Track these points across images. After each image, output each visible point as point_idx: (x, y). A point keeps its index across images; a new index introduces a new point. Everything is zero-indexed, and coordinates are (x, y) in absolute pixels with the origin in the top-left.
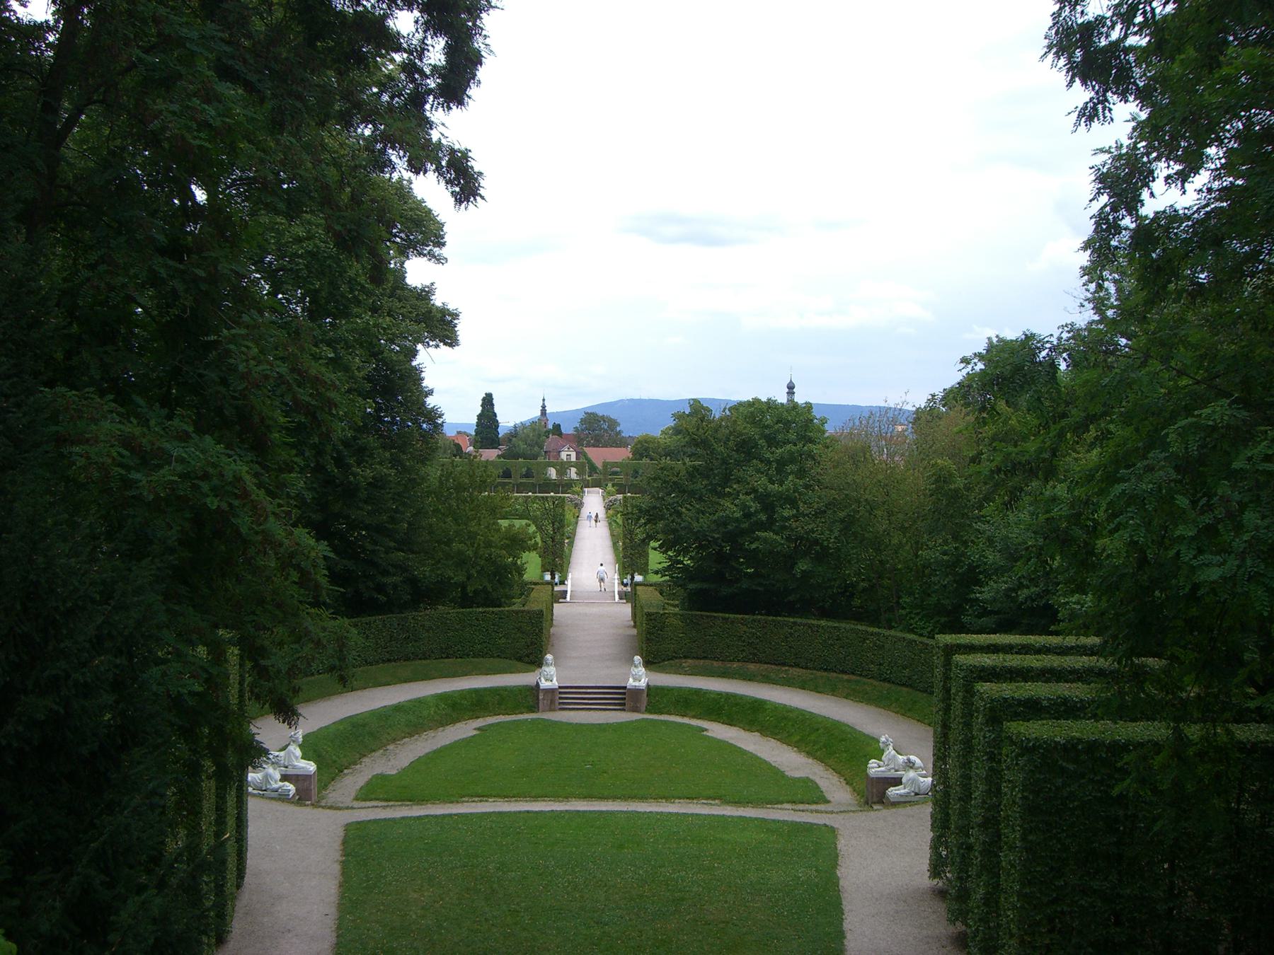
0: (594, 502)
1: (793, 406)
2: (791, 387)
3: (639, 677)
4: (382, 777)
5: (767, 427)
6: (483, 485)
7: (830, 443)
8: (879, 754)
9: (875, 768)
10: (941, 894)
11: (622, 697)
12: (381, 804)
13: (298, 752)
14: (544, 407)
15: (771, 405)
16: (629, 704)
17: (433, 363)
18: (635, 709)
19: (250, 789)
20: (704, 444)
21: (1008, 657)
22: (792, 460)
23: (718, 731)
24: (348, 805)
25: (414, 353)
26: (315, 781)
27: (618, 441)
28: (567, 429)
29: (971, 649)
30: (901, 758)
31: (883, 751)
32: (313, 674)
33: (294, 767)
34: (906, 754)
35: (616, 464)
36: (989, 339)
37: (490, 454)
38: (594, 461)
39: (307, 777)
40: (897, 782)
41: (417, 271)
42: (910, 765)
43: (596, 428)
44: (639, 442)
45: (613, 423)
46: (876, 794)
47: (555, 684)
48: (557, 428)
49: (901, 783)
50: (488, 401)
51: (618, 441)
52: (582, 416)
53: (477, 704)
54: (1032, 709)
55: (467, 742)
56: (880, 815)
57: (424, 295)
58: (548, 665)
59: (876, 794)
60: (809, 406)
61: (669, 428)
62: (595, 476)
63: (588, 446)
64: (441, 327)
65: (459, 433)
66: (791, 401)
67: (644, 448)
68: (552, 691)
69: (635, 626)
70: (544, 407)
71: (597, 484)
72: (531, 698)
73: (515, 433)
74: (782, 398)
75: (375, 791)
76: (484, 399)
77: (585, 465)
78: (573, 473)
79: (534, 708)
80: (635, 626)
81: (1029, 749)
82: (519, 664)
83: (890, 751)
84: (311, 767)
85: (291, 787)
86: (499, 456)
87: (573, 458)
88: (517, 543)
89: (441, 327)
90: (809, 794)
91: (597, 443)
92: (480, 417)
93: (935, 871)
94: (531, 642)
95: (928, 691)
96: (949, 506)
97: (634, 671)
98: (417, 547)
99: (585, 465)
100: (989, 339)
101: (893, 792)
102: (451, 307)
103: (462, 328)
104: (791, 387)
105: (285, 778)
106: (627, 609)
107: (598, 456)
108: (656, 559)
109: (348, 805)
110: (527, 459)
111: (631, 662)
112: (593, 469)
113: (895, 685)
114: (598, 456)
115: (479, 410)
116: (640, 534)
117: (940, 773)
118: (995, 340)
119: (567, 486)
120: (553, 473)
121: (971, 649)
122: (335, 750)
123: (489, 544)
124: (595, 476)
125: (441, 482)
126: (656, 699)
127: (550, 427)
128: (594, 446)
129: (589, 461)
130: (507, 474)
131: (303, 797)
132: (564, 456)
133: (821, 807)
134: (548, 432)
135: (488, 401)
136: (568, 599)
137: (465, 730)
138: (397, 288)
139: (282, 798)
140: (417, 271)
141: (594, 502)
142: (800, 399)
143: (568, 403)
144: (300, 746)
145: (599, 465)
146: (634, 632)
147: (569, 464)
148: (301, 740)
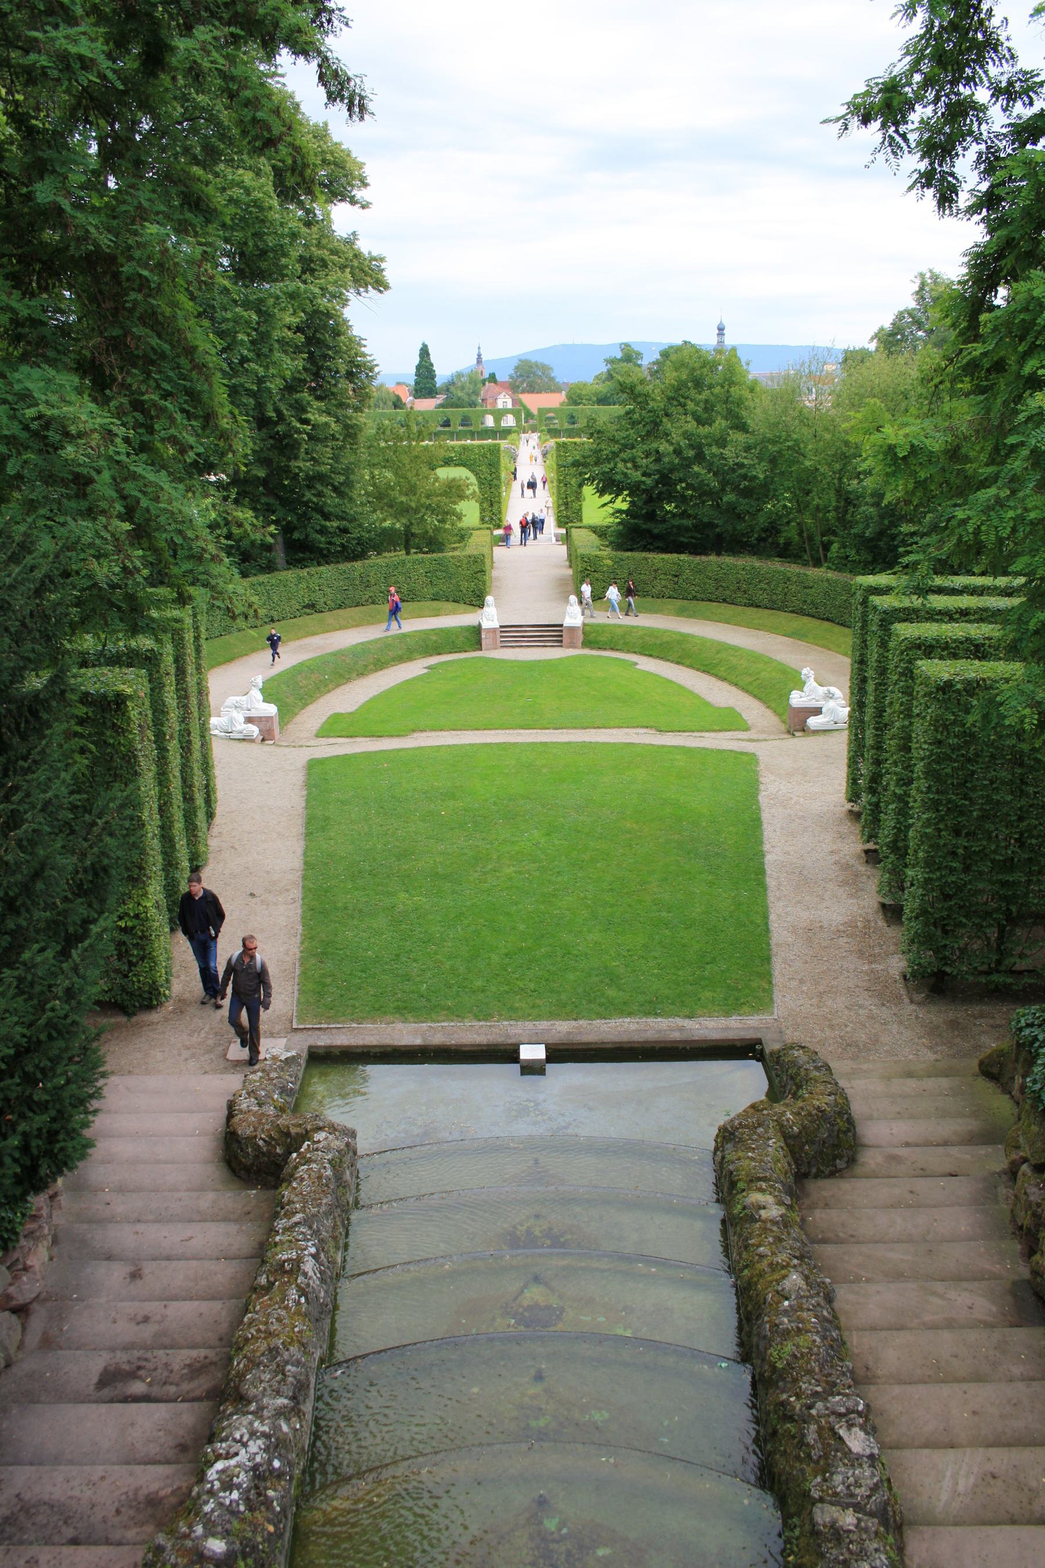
2: (721, 330)
4: (336, 718)
8: (800, 685)
9: (797, 699)
10: (855, 816)
11: (554, 634)
13: (260, 697)
14: (479, 355)
15: (696, 350)
16: (566, 639)
17: (362, 316)
18: (572, 645)
24: (308, 741)
25: (345, 302)
26: (276, 720)
27: (552, 387)
28: (503, 377)
30: (822, 690)
31: (804, 683)
34: (827, 694)
35: (549, 410)
37: (426, 405)
39: (269, 719)
40: (817, 711)
41: (342, 218)
42: (830, 696)
43: (529, 376)
45: (545, 369)
46: (797, 723)
47: (496, 624)
48: (492, 378)
50: (424, 352)
51: (552, 387)
52: (516, 363)
55: (419, 679)
56: (800, 743)
59: (797, 723)
62: (531, 422)
63: (523, 392)
64: (368, 275)
65: (398, 384)
66: (721, 342)
67: (575, 398)
68: (494, 630)
70: (479, 355)
72: (475, 637)
75: (336, 727)
79: (478, 645)
82: (450, 605)
83: (811, 684)
84: (271, 709)
85: (254, 730)
87: (510, 406)
88: (455, 490)
89: (368, 275)
90: (730, 721)
91: (532, 389)
92: (418, 368)
93: (853, 796)
97: (569, 609)
98: (324, 498)
99: (519, 410)
101: (813, 722)
103: (390, 274)
104: (721, 330)
105: (249, 720)
106: (563, 550)
107: (534, 402)
109: (308, 741)
110: (456, 403)
111: (567, 600)
112: (529, 415)
113: (826, 611)
114: (534, 402)
117: (858, 705)
118: (928, 275)
119: (506, 433)
120: (490, 421)
122: (290, 694)
124: (528, 421)
126: (591, 638)
127: (486, 375)
130: (447, 424)
131: (266, 736)
134: (483, 382)
135: (424, 352)
137: (416, 668)
139: (246, 740)
140: (342, 218)
142: (729, 341)
143: (504, 349)
145: (535, 412)
146: (570, 572)
147: (505, 412)
148: (261, 685)
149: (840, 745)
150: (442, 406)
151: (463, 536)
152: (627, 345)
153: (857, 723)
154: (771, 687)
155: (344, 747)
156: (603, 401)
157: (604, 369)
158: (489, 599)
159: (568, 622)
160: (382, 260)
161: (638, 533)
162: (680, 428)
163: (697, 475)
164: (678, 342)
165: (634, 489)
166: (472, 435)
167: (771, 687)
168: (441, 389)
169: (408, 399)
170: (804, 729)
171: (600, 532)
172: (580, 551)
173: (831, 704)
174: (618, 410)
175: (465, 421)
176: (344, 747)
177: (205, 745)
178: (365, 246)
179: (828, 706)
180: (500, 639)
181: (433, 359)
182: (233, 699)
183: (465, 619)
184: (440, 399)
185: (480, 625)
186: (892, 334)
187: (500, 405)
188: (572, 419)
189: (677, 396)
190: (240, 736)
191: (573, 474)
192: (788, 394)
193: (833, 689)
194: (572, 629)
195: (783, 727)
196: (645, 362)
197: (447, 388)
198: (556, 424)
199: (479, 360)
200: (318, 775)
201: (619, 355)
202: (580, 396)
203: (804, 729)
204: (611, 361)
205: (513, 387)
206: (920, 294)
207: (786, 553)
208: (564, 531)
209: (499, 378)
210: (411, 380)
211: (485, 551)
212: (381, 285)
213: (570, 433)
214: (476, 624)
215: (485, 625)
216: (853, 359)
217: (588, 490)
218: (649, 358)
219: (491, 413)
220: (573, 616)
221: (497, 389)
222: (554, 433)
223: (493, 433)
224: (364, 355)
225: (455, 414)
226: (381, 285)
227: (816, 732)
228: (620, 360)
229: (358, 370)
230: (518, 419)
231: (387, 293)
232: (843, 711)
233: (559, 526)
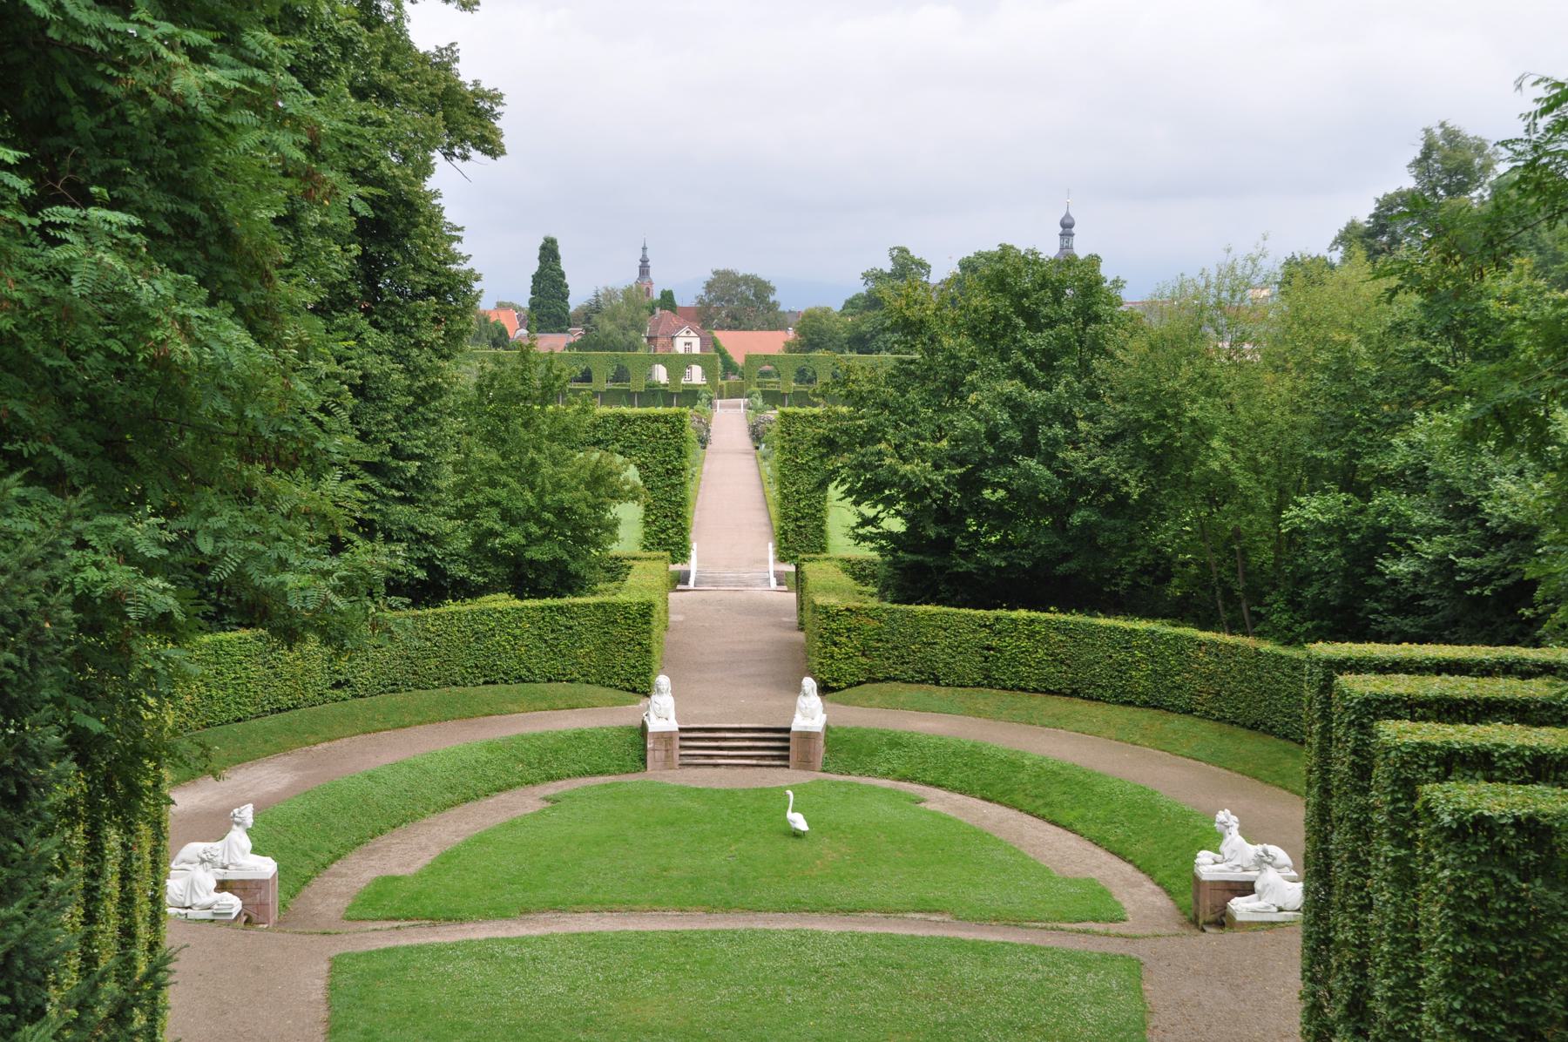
0: (729, 422)
2: (1067, 226)
3: (810, 713)
6: (548, 393)
7: (1133, 324)
8: (1213, 840)
9: (1207, 866)
12: (388, 925)
13: (246, 844)
15: (1031, 261)
17: (454, 185)
19: (170, 911)
20: (911, 328)
22: (1066, 349)
23: (940, 801)
25: (425, 169)
28: (685, 299)
30: (1254, 850)
37: (552, 343)
38: (730, 353)
39: (259, 884)
40: (1246, 888)
42: (1262, 862)
43: (738, 301)
47: (672, 725)
48: (667, 299)
49: (1252, 891)
50: (549, 252)
53: (545, 762)
54: (1482, 763)
57: (443, 62)
59: (1209, 909)
60: (1094, 261)
61: (858, 297)
63: (721, 328)
67: (813, 333)
69: (801, 627)
71: (736, 393)
72: (637, 745)
73: (592, 311)
74: (1049, 249)
75: (379, 902)
76: (543, 248)
78: (696, 376)
80: (801, 627)
81: (1472, 830)
83: (1234, 839)
84: (265, 867)
85: (232, 903)
86: (570, 346)
87: (696, 349)
89: (467, 119)
91: (736, 322)
92: (537, 279)
94: (625, 654)
97: (802, 701)
101: (1241, 907)
102: (486, 86)
103: (507, 123)
104: (1067, 226)
105: (222, 886)
108: (841, 514)
111: (798, 689)
112: (729, 367)
113: (1252, 715)
114: (740, 344)
115: (535, 266)
116: (806, 482)
118: (1438, 132)
120: (661, 374)
123: (558, 486)
124: (730, 376)
125: (479, 387)
126: (845, 750)
127: (656, 295)
128: (730, 328)
129: (723, 353)
132: (679, 347)
133: (1114, 928)
135: (549, 252)
137: (526, 802)
141: (729, 422)
142: (1081, 250)
144: (248, 831)
145: (739, 360)
147: (688, 360)
150: (580, 346)
151: (616, 570)
154: (1162, 845)
155: (380, 938)
156: (861, 343)
158: (663, 680)
159: (799, 724)
160: (496, 98)
162: (990, 396)
165: (915, 493)
166: (630, 397)
168: (577, 316)
169: (518, 333)
171: (858, 571)
174: (886, 360)
175: (620, 375)
176: (380, 938)
177: (155, 920)
178: (467, 72)
180: (677, 743)
181: (565, 265)
182: (195, 848)
183: (602, 716)
184: (576, 334)
186: (1371, 234)
187: (679, 347)
188: (803, 376)
189: (990, 334)
190: (207, 915)
191: (804, 470)
193: (1273, 849)
194: (807, 736)
198: (773, 384)
199: (644, 269)
201: (888, 266)
204: (875, 277)
205: (703, 317)
206: (1422, 163)
208: (792, 569)
210: (522, 296)
211: (655, 598)
213: (802, 399)
214: (637, 723)
215: (655, 725)
216: (1302, 274)
218: (942, 268)
219: (664, 361)
220: (810, 713)
224: (454, 258)
225: (601, 362)
228: (889, 275)
233: (782, 560)
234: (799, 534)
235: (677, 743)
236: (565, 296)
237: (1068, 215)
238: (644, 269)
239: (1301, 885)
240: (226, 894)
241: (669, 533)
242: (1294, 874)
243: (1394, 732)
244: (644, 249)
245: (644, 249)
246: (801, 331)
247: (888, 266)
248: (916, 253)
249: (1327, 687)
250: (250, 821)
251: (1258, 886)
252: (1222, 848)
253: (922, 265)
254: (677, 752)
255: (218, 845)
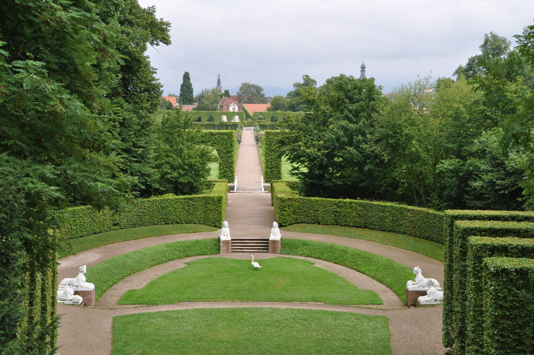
0: (248, 135)
1: (364, 80)
2: (363, 68)
3: (276, 234)
5: (349, 91)
6: (186, 125)
7: (386, 101)
8: (413, 277)
9: (411, 286)
12: (132, 306)
13: (84, 278)
15: (351, 80)
16: (270, 248)
17: (154, 54)
18: (274, 251)
21: (506, 223)
22: (363, 110)
23: (320, 264)
25: (144, 49)
27: (263, 100)
28: (233, 93)
29: (462, 218)
30: (426, 280)
32: (299, 110)
33: (81, 286)
36: (486, 35)
37: (188, 108)
38: (248, 111)
40: (424, 293)
42: (431, 284)
43: (250, 94)
44: (275, 99)
47: (229, 238)
48: (227, 93)
49: (426, 294)
50: (186, 77)
51: (263, 100)
53: (185, 251)
54: (504, 251)
58: (224, 227)
59: (412, 300)
61: (292, 92)
62: (249, 120)
67: (276, 104)
69: (273, 205)
70: (219, 80)
71: (250, 125)
72: (217, 245)
74: (357, 76)
75: (130, 298)
76: (184, 76)
77: (245, 115)
78: (237, 119)
80: (273, 205)
83: (420, 276)
84: (91, 286)
87: (237, 110)
90: (374, 300)
91: (250, 101)
92: (182, 86)
94: (212, 214)
95: (441, 242)
96: (460, 136)
97: (273, 230)
99: (245, 115)
100: (486, 35)
101: (422, 299)
102: (165, 20)
103: (172, 33)
104: (363, 68)
105: (76, 293)
108: (286, 166)
111: (271, 226)
112: (248, 116)
113: (426, 234)
114: (252, 108)
115: (182, 82)
117: (448, 287)
118: (490, 35)
119: (235, 126)
120: (225, 119)
121: (462, 218)
122: (104, 278)
123: (190, 157)
124: (248, 119)
125: (163, 123)
126: (287, 246)
127: (223, 92)
128: (248, 103)
129: (246, 111)
132: (231, 109)
135: (186, 77)
136: (235, 190)
137: (179, 264)
138: (134, 7)
141: (248, 135)
142: (368, 76)
144: (85, 274)
145: (251, 114)
147: (234, 114)
149: (439, 314)
151: (210, 185)
152: (307, 76)
153: (448, 300)
154: (395, 279)
156: (293, 108)
157: (293, 89)
159: (272, 238)
160: (168, 24)
161: (314, 185)
163: (350, 152)
164: (338, 75)
165: (311, 159)
166: (214, 127)
167: (395, 279)
169: (176, 105)
170: (416, 304)
172: (279, 196)
173: (432, 289)
175: (211, 119)
177: (53, 304)
179: (431, 290)
180: (231, 244)
181: (192, 81)
182: (66, 280)
183: (205, 235)
184: (195, 105)
185: (219, 239)
186: (467, 70)
187: (231, 109)
188: (273, 119)
189: (337, 105)
190: (71, 303)
191: (273, 151)
192: (408, 98)
194: (275, 242)
195: (403, 304)
196: (318, 86)
197: (201, 97)
199: (219, 83)
200: (120, 327)
201: (302, 82)
202: (278, 105)
203: (416, 304)
205: (239, 99)
207: (401, 199)
208: (269, 185)
209: (231, 94)
211: (223, 195)
212: (166, 41)
213: (273, 127)
214: (217, 238)
215: (223, 238)
217: (284, 159)
218: (320, 83)
219: (226, 114)
220: (276, 234)
221: (230, 100)
222: (263, 127)
223: (222, 125)
224: (154, 79)
226: (166, 41)
227: (423, 306)
228: (303, 85)
229: (153, 90)
230: (241, 118)
231: (169, 46)
232: (440, 295)
233: (266, 182)
234: (272, 173)
235: (231, 244)
236: (192, 92)
237: (363, 64)
238: (219, 83)
239: (443, 292)
240: (77, 296)
241: (227, 173)
242: (440, 288)
243: (474, 240)
244: (219, 76)
245: (219, 76)
246: (272, 104)
247: (302, 82)
248: (312, 77)
249: (452, 225)
250: (85, 271)
251: (428, 292)
252: (416, 280)
253: (313, 81)
254: (230, 247)
255: (74, 279)
